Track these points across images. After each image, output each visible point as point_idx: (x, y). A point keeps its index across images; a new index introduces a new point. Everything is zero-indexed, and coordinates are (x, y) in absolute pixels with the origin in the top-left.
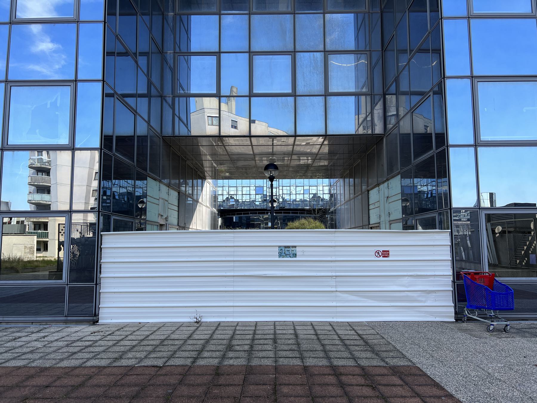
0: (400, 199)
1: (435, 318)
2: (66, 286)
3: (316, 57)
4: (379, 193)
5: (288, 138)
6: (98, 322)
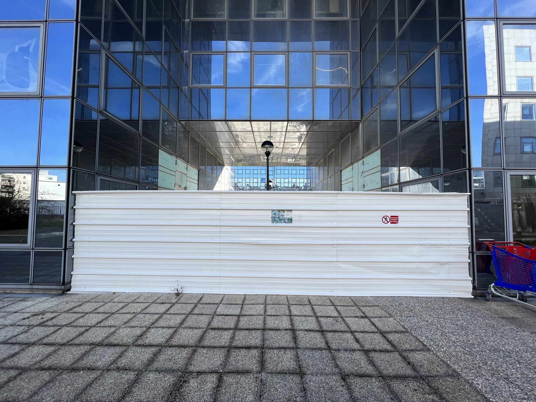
0: (379, 171)
1: (449, 293)
2: (31, 250)
3: (306, 56)
4: (352, 170)
5: (283, 122)
6: (70, 291)
